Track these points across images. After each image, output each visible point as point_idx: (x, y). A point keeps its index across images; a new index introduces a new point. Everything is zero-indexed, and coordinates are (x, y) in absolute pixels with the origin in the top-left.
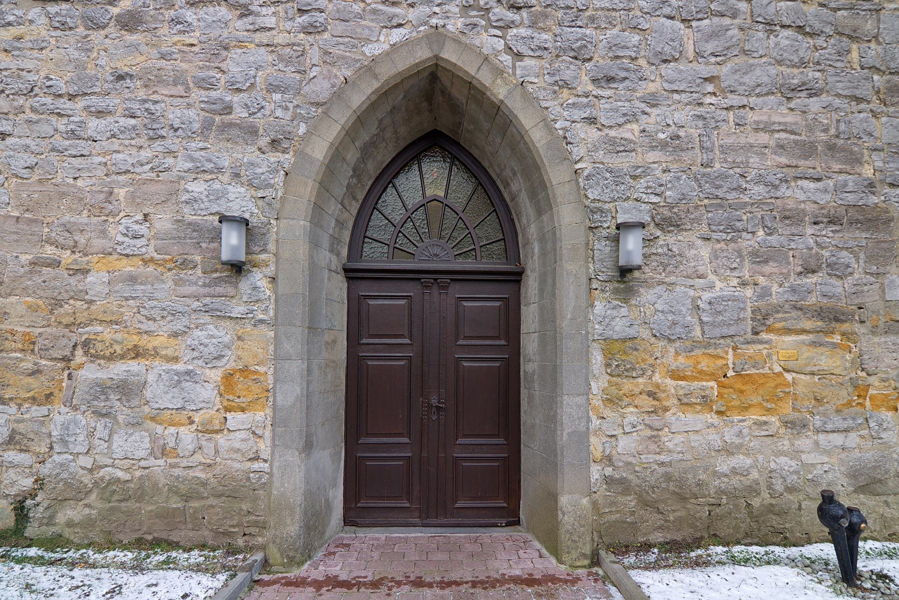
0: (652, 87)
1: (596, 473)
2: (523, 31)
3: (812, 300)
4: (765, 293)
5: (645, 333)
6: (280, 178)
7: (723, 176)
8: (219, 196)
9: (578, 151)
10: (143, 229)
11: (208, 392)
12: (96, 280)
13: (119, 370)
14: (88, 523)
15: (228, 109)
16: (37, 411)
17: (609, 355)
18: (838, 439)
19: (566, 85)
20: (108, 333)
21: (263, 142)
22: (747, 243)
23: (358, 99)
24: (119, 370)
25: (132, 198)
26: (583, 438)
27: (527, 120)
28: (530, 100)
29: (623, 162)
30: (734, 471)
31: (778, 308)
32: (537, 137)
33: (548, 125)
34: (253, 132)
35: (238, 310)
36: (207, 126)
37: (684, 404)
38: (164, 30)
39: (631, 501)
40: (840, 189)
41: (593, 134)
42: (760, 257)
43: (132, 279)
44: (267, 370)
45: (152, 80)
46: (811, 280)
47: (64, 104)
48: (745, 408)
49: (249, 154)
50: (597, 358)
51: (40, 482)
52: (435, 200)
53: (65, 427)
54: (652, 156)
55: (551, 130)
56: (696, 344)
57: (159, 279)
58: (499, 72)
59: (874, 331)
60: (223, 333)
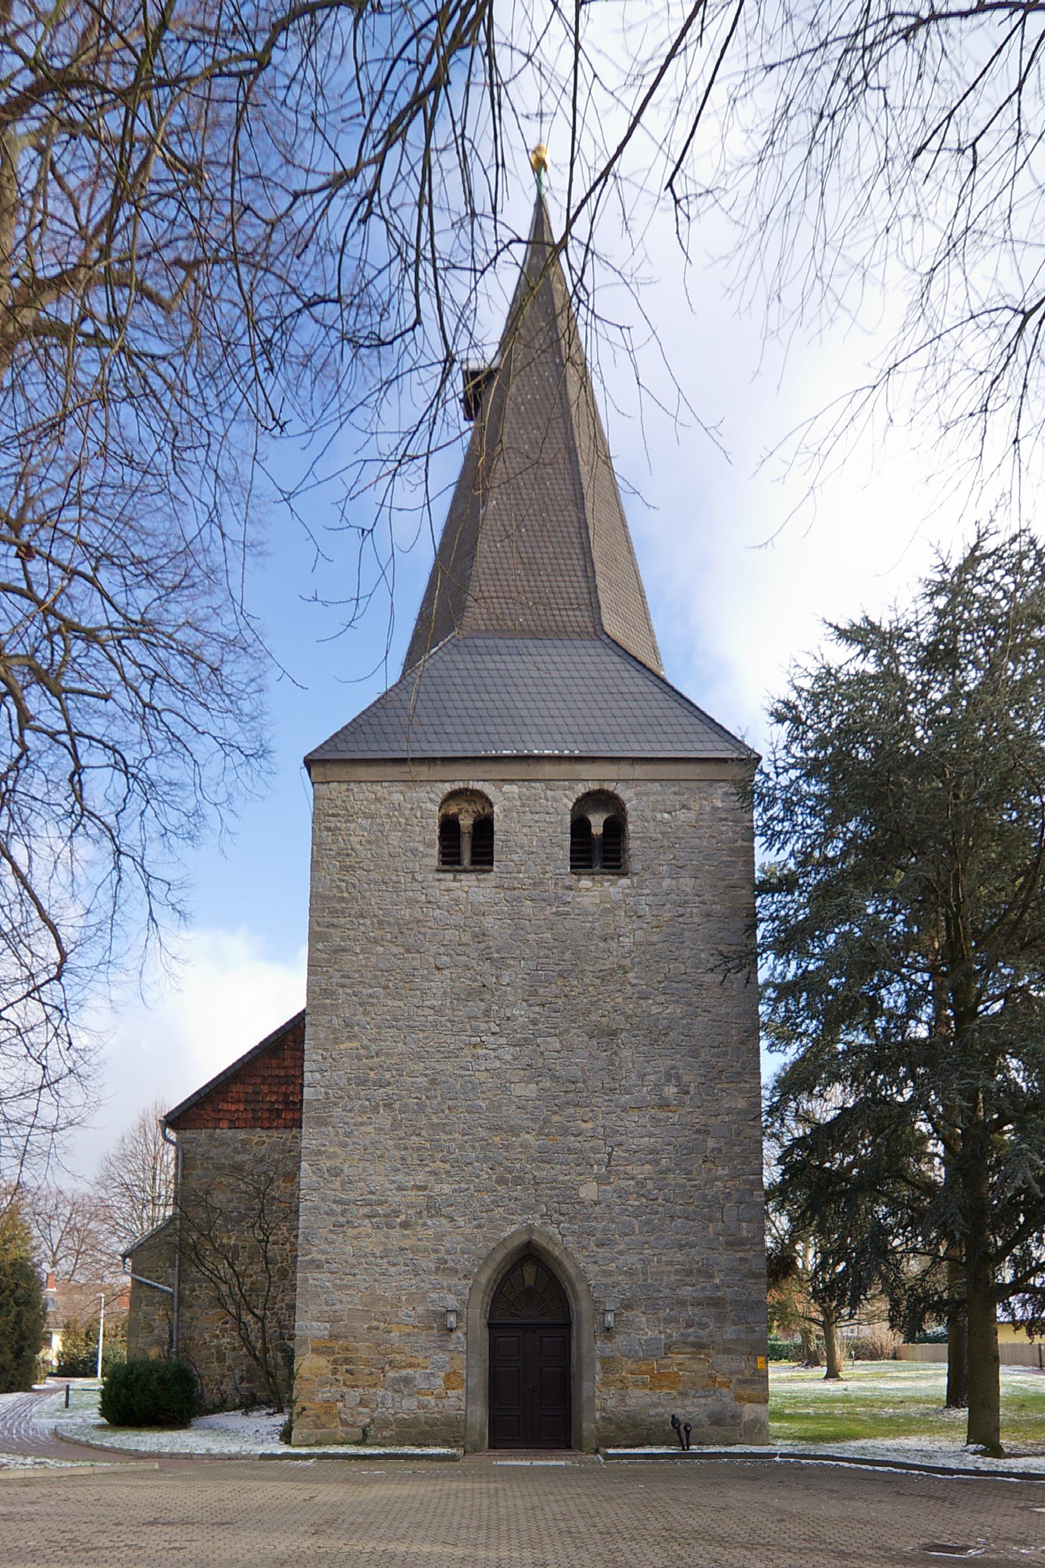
0: (621, 1247)
1: (598, 1415)
2: (566, 1225)
3: (691, 1339)
4: (670, 1336)
5: (618, 1355)
6: (467, 1292)
7: (651, 1285)
8: (442, 1299)
9: (590, 1276)
10: (413, 1313)
11: (440, 1382)
12: (395, 1335)
13: (405, 1372)
14: (391, 1437)
15: (446, 1262)
16: (372, 1391)
17: (603, 1364)
18: (703, 1401)
19: (584, 1247)
20: (398, 1357)
21: (461, 1275)
22: (662, 1314)
23: (499, 1257)
24: (405, 1372)
25: (407, 1300)
26: (592, 1399)
27: (567, 1264)
28: (569, 1255)
29: (609, 1281)
30: (657, 1415)
31: (676, 1343)
32: (572, 1272)
33: (577, 1267)
34: (456, 1271)
35: (452, 1347)
36: (438, 1269)
37: (636, 1385)
38: (419, 1228)
39: (613, 1427)
40: (704, 1289)
41: (597, 1268)
42: (667, 1321)
43: (408, 1335)
44: (463, 1372)
45: (415, 1250)
46: (691, 1330)
47: (379, 1261)
48: (661, 1387)
49: (454, 1281)
50: (598, 1366)
51: (373, 1420)
52: (670, 185)
53: (383, 1396)
54: (621, 1278)
55: (577, 1267)
56: (640, 1359)
57: (419, 1334)
58: (556, 1244)
59: (718, 1352)
60: (444, 1357)
